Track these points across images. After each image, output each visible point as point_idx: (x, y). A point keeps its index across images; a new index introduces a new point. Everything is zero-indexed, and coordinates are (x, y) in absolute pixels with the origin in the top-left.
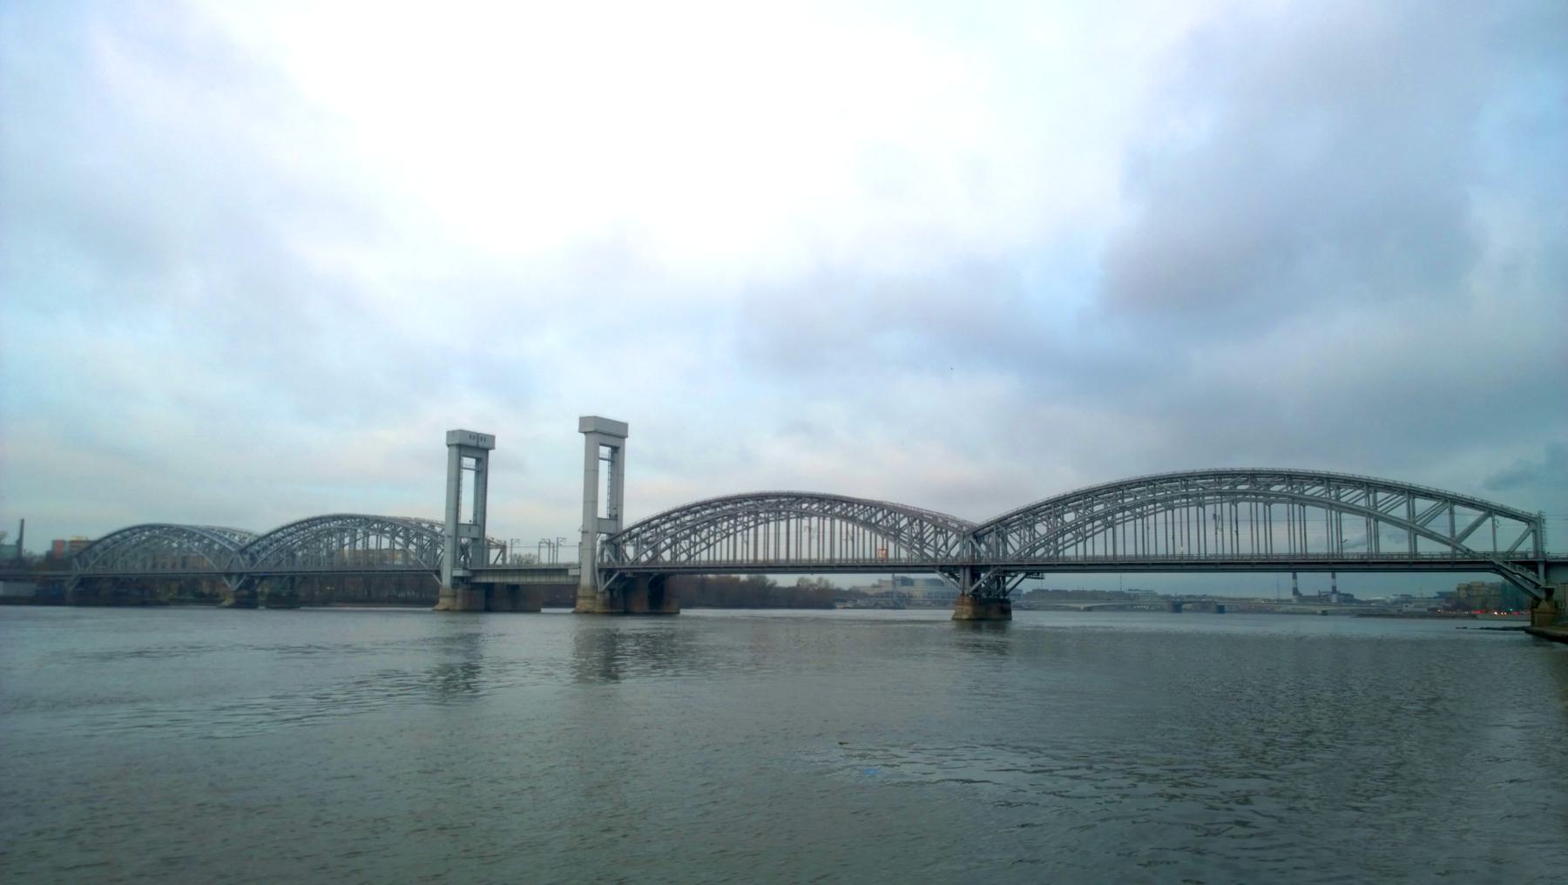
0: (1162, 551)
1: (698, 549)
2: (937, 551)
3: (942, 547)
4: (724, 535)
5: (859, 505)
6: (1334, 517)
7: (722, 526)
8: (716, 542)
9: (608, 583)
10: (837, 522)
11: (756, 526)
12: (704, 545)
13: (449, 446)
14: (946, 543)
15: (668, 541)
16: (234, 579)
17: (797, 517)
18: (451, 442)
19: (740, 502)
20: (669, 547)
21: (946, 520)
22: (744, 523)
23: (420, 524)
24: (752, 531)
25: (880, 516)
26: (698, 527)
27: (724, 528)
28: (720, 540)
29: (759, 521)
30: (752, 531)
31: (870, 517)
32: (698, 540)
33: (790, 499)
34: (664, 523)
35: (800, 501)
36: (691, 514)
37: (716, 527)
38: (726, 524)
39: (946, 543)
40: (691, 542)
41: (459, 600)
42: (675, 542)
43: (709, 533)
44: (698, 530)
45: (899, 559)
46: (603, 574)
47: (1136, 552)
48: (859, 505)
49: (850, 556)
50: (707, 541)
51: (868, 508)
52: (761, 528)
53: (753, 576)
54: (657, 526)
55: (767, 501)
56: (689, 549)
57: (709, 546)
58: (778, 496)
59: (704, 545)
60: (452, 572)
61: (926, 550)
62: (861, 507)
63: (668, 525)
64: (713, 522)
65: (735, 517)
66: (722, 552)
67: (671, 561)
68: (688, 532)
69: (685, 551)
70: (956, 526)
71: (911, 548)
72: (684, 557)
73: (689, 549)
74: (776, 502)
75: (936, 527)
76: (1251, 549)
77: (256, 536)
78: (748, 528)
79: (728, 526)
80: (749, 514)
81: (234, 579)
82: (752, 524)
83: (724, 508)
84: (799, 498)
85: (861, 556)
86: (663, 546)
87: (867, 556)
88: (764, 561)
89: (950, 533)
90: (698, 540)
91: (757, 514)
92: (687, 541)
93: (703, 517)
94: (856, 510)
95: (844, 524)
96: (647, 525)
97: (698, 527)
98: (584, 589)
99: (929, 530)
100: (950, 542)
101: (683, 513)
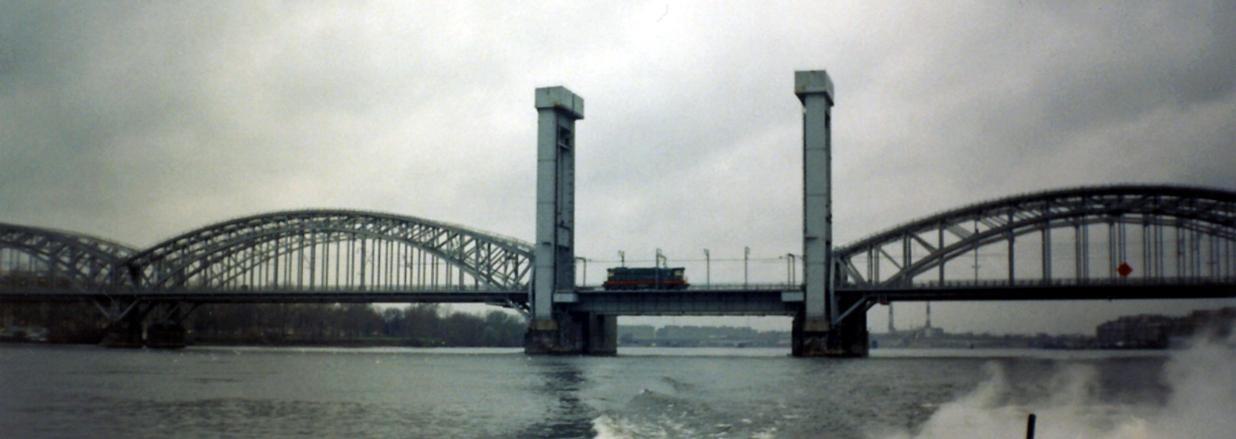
0: (342, 282)
1: (232, 273)
2: (506, 278)
3: (510, 274)
4: (263, 258)
5: (421, 225)
6: (402, 251)
7: (261, 247)
8: (253, 266)
9: (847, 313)
10: (369, 242)
11: (301, 248)
12: (239, 270)
13: (540, 109)
14: (516, 271)
15: (197, 264)
16: (116, 306)
17: (349, 239)
18: (545, 104)
19: (283, 221)
20: (198, 271)
21: (515, 244)
22: (287, 245)
23: (96, 244)
24: (295, 254)
25: (443, 238)
26: (232, 249)
27: (264, 250)
28: (260, 263)
29: (305, 243)
30: (295, 254)
31: (432, 240)
32: (232, 263)
33: (342, 218)
34: (193, 243)
35: (352, 220)
36: (225, 232)
37: (254, 249)
38: (265, 245)
39: (516, 271)
40: (223, 265)
42: (205, 265)
43: (244, 256)
44: (233, 252)
45: (437, 286)
47: (584, 281)
48: (421, 225)
49: (402, 283)
50: (242, 265)
51: (431, 229)
52: (307, 251)
53: (416, 305)
54: (184, 247)
55: (315, 219)
56: (222, 274)
57: (244, 271)
58: (328, 213)
59: (239, 270)
60: (552, 298)
61: (494, 277)
62: (423, 228)
63: (197, 246)
64: (250, 242)
65: (277, 237)
66: (260, 278)
67: (218, 287)
68: (220, 254)
69: (216, 276)
70: (527, 250)
71: (477, 274)
72: (215, 281)
73: (222, 274)
74: (325, 221)
75: (506, 252)
76: (705, 275)
77: (132, 250)
78: (290, 251)
79: (268, 248)
80: (292, 234)
81: (116, 306)
82: (295, 246)
83: (289, 222)
84: (351, 216)
85: (294, 281)
86: (191, 269)
87: (402, 283)
88: (347, 286)
89: (521, 258)
90: (232, 263)
91: (302, 233)
92: (219, 265)
93: (238, 236)
94: (416, 232)
95: (403, 246)
96: (172, 245)
97: (232, 249)
98: (815, 321)
99: (497, 252)
100: (521, 269)
101: (192, 239)
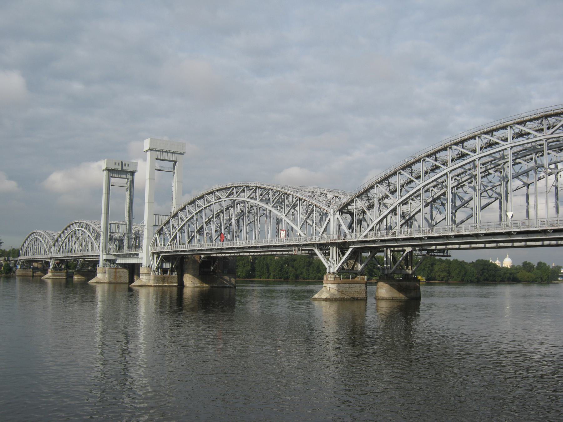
41: (107, 275)
46: (155, 256)
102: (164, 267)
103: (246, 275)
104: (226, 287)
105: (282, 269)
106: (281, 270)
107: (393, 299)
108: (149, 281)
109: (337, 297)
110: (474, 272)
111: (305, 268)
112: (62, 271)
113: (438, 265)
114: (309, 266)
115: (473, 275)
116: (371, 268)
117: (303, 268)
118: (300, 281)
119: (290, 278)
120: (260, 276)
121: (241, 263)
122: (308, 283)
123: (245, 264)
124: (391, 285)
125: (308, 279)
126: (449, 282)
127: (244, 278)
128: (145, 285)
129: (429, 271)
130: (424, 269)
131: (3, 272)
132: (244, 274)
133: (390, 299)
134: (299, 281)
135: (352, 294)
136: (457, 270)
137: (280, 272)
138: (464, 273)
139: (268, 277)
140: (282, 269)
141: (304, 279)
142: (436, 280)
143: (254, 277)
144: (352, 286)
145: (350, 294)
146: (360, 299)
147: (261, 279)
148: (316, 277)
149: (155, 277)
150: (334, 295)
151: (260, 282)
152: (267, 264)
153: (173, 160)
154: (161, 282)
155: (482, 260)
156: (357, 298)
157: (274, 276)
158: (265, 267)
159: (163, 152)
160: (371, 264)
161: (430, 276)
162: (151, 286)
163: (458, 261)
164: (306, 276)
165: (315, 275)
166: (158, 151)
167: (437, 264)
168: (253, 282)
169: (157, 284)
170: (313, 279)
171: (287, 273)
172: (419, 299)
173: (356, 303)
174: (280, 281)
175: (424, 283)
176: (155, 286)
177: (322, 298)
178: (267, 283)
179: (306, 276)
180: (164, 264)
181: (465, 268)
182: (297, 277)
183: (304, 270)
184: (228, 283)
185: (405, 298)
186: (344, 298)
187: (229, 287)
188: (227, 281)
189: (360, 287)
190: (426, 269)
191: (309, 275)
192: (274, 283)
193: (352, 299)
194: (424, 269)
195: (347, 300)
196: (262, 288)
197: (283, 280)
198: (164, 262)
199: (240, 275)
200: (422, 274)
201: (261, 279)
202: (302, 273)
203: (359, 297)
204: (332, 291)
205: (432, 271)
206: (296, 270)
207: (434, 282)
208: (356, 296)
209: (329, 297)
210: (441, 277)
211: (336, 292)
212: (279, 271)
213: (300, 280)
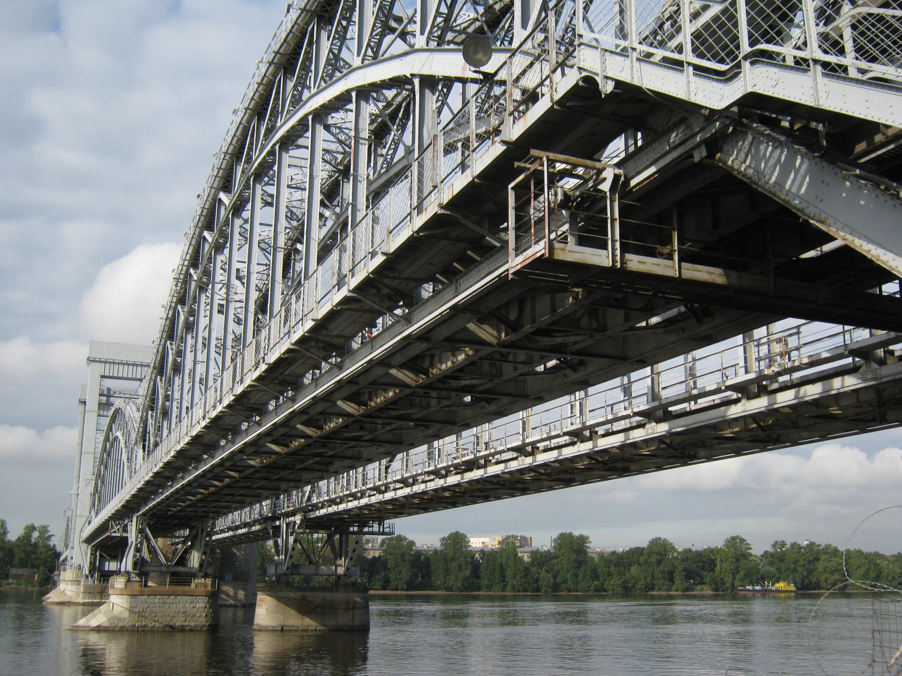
102: (106, 569)
103: (463, 585)
104: (225, 606)
105: (527, 574)
106: (525, 576)
107: (282, 630)
108: (78, 594)
109: (126, 623)
110: (894, 572)
111: (571, 571)
112: (188, 583)
113: (824, 560)
114: (579, 568)
115: (894, 578)
116: (696, 569)
117: (568, 571)
118: (563, 595)
119: (543, 590)
120: (490, 588)
121: (454, 564)
122: (577, 599)
123: (460, 566)
124: (279, 599)
125: (577, 591)
126: (848, 591)
127: (461, 591)
128: (69, 602)
129: (805, 573)
130: (795, 570)
131: (35, 584)
132: (459, 584)
133: (276, 631)
134: (559, 595)
135: (168, 619)
136: (862, 568)
137: (523, 580)
138: (874, 575)
139: (504, 590)
140: (527, 574)
141: (569, 591)
142: (822, 589)
143: (479, 589)
144: (169, 601)
145: (162, 616)
146: (191, 630)
147: (492, 593)
148: (590, 587)
149: (86, 586)
150: (119, 619)
151: (491, 599)
152: (501, 566)
153: (134, 377)
154: (98, 596)
155: (828, 546)
156: (182, 626)
157: (514, 587)
158: (498, 571)
159: (114, 363)
160: (698, 562)
161: (807, 581)
162: (77, 604)
163: (862, 553)
164: (572, 586)
165: (588, 584)
166: (105, 362)
167: (822, 558)
168: (476, 598)
169: (90, 601)
170: (586, 591)
171: (537, 580)
172: (364, 630)
173: (178, 638)
174: (525, 595)
175: (793, 594)
176: (84, 604)
177: (90, 627)
178: (503, 598)
179: (572, 586)
180: (107, 563)
181: (876, 565)
182: (556, 587)
183: (569, 575)
184: (228, 599)
185: (318, 628)
186: (145, 626)
187: (230, 606)
188: (228, 595)
189: (192, 602)
190: (798, 568)
191: (578, 584)
192: (515, 599)
193: (167, 629)
194: (795, 570)
195: (153, 631)
196: (774, 609)
197: (529, 593)
198: (107, 560)
199: (453, 586)
200: (791, 577)
201: (492, 593)
202: (565, 582)
203: (187, 623)
204: (117, 610)
205: (811, 572)
206: (555, 578)
207: (816, 591)
208: (178, 622)
209: (107, 624)
210: (829, 582)
211: (126, 614)
212: (522, 578)
213: (562, 593)
